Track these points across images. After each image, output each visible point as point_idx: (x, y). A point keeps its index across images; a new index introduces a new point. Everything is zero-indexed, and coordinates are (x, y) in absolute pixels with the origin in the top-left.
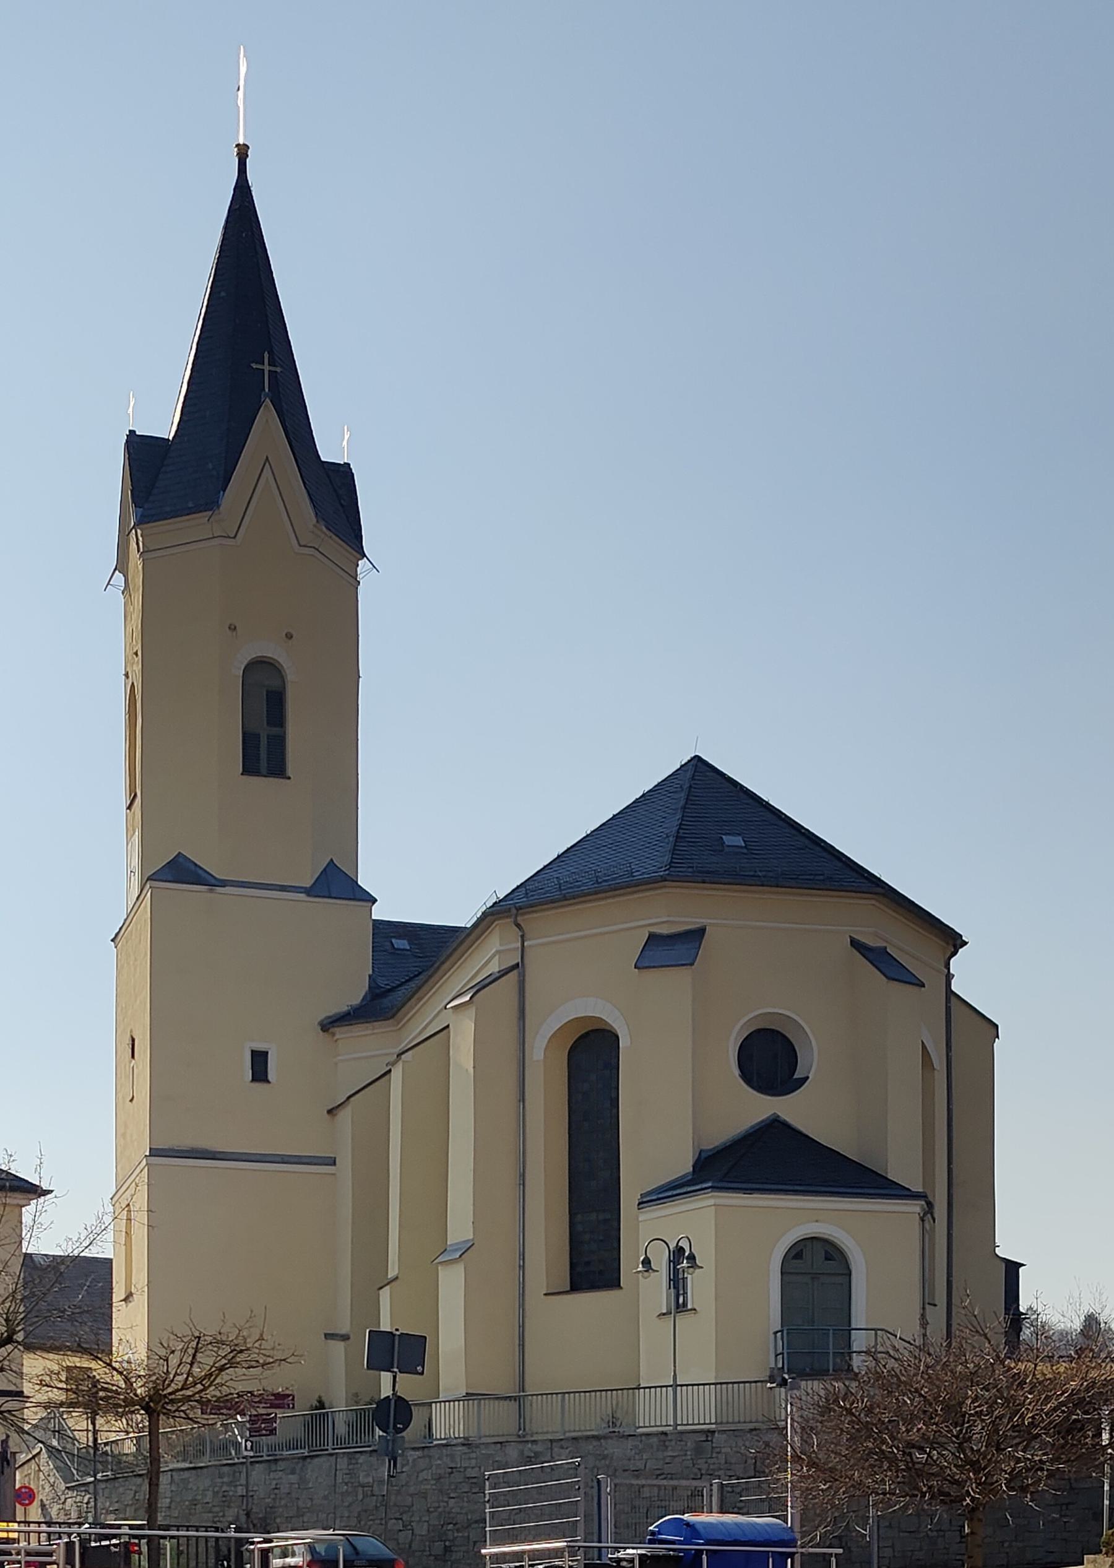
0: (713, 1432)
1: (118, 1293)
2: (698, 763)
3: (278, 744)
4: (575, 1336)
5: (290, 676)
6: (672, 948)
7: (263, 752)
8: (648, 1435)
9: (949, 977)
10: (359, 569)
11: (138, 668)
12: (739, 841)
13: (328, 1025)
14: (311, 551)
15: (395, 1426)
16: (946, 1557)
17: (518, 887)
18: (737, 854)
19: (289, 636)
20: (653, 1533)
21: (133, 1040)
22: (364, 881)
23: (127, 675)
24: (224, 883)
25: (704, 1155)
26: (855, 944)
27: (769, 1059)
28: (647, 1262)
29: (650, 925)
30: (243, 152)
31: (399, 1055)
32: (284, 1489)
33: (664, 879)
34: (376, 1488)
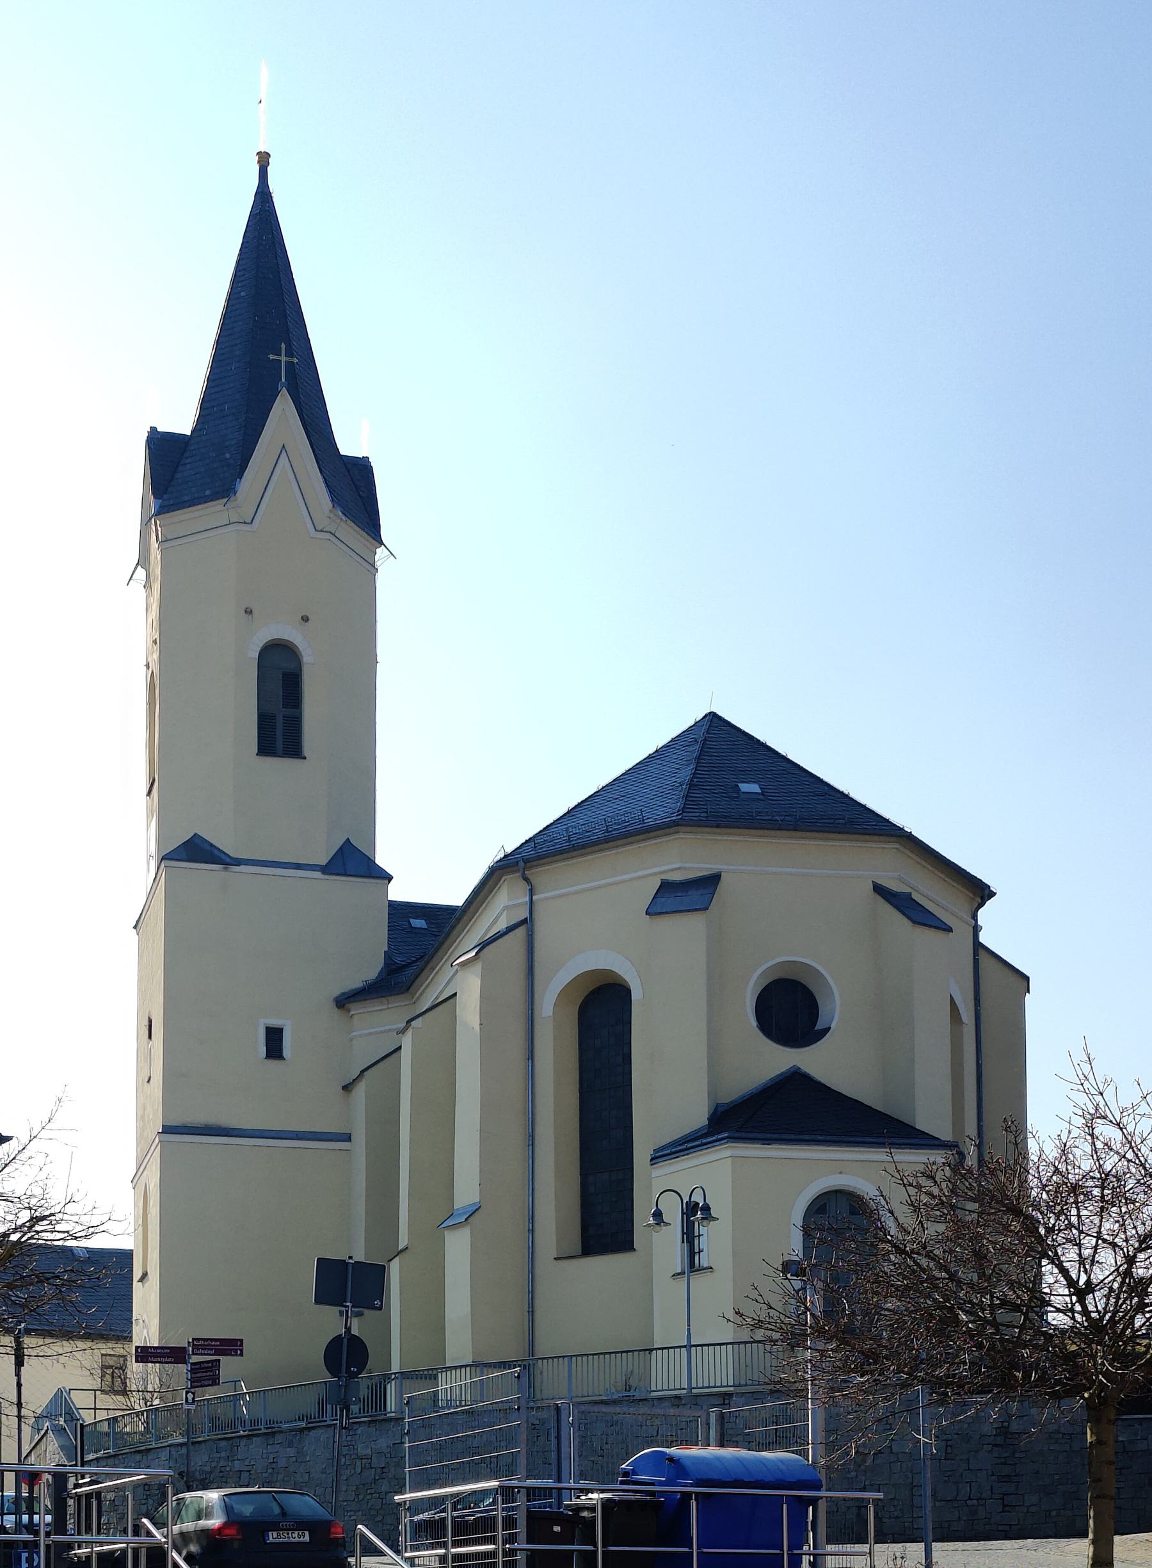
0: (730, 1395)
1: (137, 1274)
2: (713, 721)
3: (294, 727)
4: (586, 1300)
5: (307, 658)
6: (685, 895)
7: (280, 728)
8: (660, 1399)
9: (976, 929)
10: (377, 557)
11: (156, 656)
12: (755, 788)
13: (344, 1001)
14: (328, 536)
15: (348, 1371)
16: (987, 1527)
17: (527, 842)
18: (753, 800)
19: (305, 619)
20: (626, 1474)
21: (150, 1021)
22: (382, 859)
23: (148, 666)
24: (238, 862)
25: (720, 1110)
26: (879, 889)
27: (789, 1009)
28: (658, 1215)
29: (660, 873)
30: (264, 160)
31: (409, 1022)
32: (282, 1463)
33: (676, 824)
34: (374, 1460)
